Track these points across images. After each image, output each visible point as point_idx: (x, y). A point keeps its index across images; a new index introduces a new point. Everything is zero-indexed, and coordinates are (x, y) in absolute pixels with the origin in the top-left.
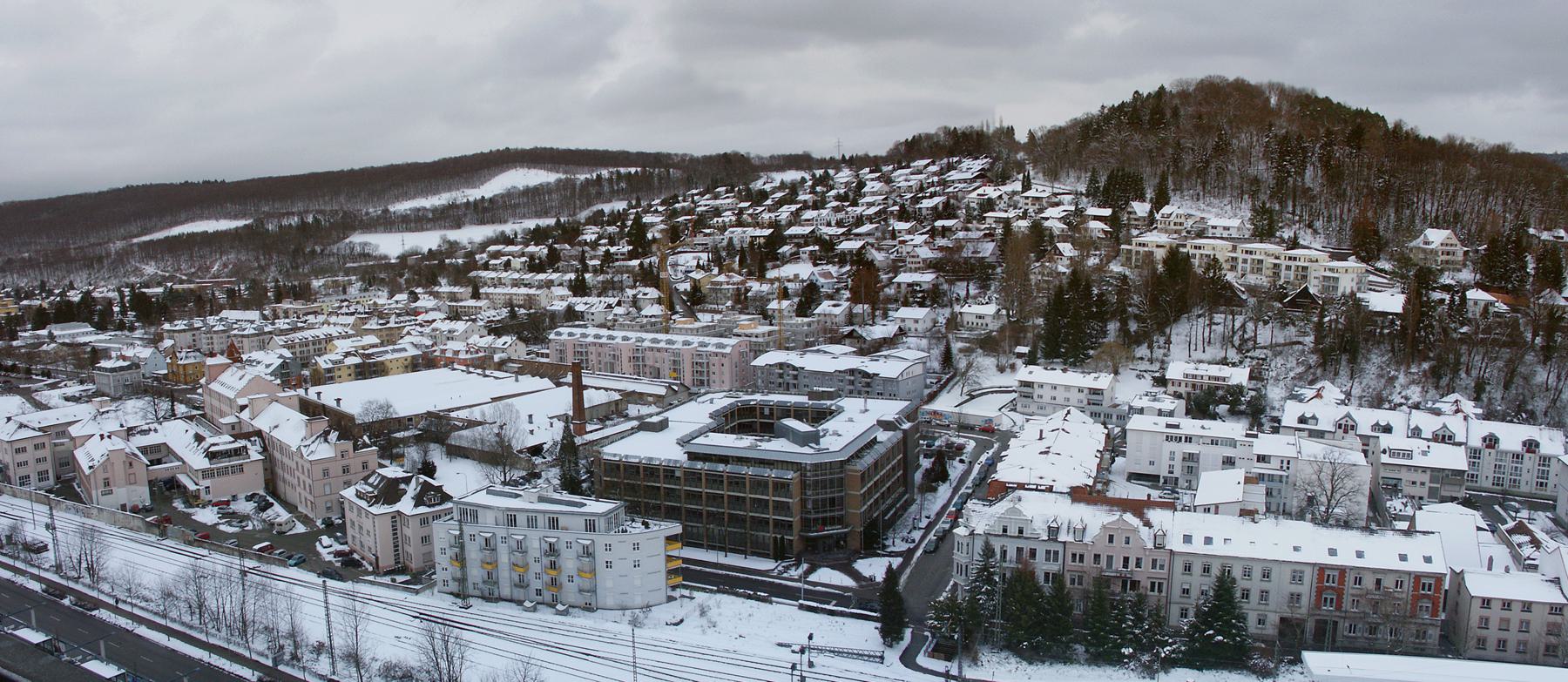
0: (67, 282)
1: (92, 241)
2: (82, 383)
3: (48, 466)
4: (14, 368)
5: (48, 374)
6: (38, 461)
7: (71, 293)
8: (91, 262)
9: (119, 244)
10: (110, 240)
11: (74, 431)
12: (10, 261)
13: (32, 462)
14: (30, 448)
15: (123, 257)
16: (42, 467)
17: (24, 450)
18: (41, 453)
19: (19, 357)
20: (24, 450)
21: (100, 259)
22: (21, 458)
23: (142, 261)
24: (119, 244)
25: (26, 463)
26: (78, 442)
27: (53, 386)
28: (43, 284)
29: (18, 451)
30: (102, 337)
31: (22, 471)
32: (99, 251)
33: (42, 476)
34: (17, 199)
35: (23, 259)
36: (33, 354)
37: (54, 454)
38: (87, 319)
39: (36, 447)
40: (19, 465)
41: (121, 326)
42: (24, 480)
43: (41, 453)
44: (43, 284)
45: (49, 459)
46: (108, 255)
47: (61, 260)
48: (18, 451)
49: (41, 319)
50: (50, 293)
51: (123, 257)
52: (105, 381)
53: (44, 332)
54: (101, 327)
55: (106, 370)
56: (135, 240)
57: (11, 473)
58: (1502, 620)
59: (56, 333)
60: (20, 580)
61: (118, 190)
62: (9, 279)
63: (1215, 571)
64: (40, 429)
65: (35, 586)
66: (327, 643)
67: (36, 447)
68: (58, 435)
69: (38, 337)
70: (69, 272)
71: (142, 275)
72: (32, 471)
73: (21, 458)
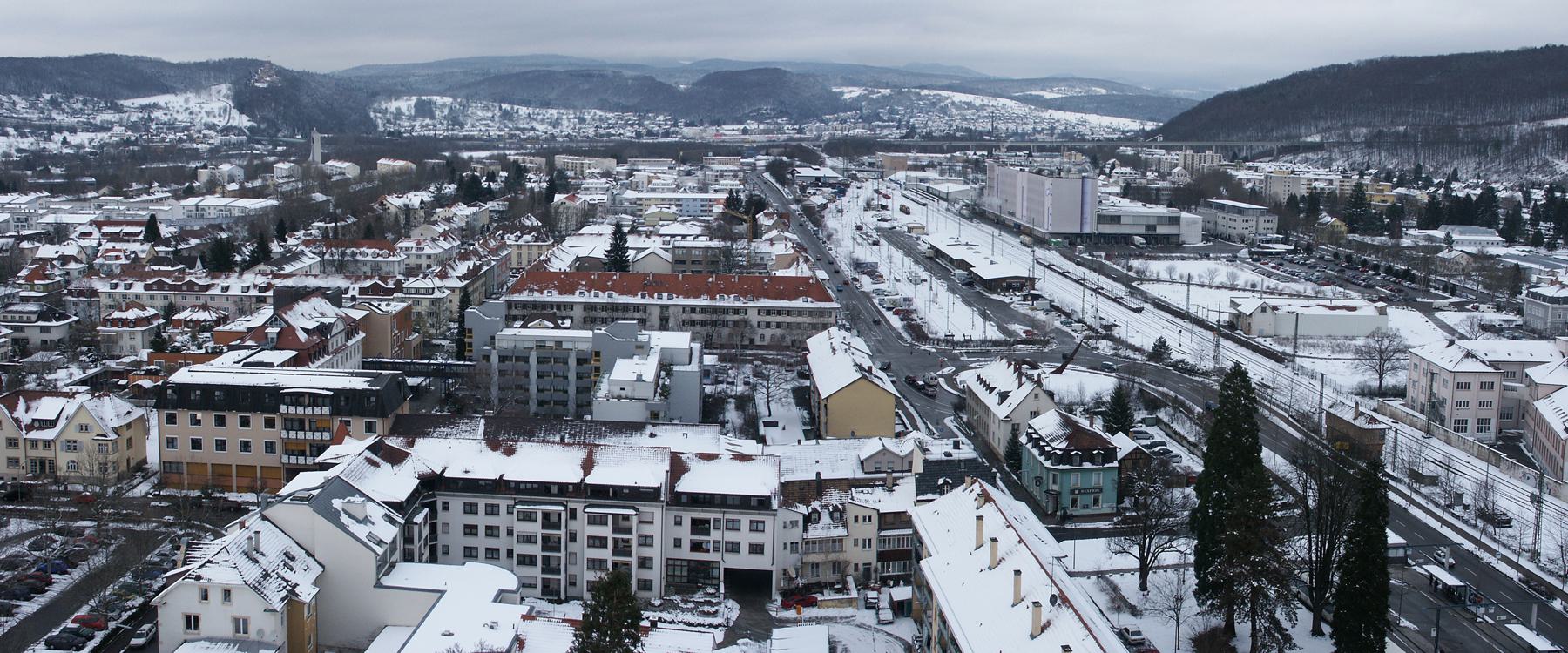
0: (1449, 170)
1: (1489, 118)
2: (1499, 308)
3: (1492, 414)
4: (1406, 275)
5: (1453, 291)
6: (1482, 404)
7: (1455, 185)
8: (1485, 147)
9: (1527, 127)
10: (1511, 122)
11: (1535, 373)
12: (1380, 134)
13: (1473, 404)
14: (1475, 386)
15: (1530, 145)
16: (1484, 413)
17: (1468, 386)
18: (1487, 396)
19: (1410, 260)
20: (1468, 386)
21: (1497, 145)
22: (1462, 395)
23: (1555, 153)
24: (1527, 127)
25: (1466, 404)
26: (1542, 392)
27: (1460, 307)
28: (1418, 169)
29: (1460, 386)
30: (1512, 250)
31: (1462, 414)
32: (1497, 132)
33: (1483, 425)
34: (1399, 53)
35: (1397, 133)
36: (1428, 256)
37: (1502, 398)
38: (1490, 223)
39: (1483, 386)
40: (1458, 404)
41: (1537, 240)
42: (1461, 426)
43: (1487, 396)
44: (1418, 169)
45: (1495, 405)
46: (1509, 140)
47: (1444, 140)
48: (1460, 386)
49: (1433, 215)
50: (1428, 183)
51: (1530, 145)
52: (1540, 313)
53: (1439, 234)
54: (1510, 238)
55: (1545, 298)
56: (1549, 123)
57: (1446, 412)
58: (476, 527)
59: (1455, 237)
60: (1486, 557)
61: (1534, 50)
62: (1376, 157)
63: (861, 567)
64: (1491, 364)
65: (1512, 573)
66: (1056, 592)
67: (1483, 386)
68: (1510, 375)
69: (1430, 238)
70: (1452, 158)
71: (1553, 173)
72: (1471, 415)
73: (1462, 395)
